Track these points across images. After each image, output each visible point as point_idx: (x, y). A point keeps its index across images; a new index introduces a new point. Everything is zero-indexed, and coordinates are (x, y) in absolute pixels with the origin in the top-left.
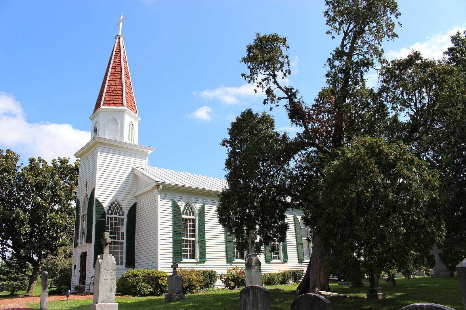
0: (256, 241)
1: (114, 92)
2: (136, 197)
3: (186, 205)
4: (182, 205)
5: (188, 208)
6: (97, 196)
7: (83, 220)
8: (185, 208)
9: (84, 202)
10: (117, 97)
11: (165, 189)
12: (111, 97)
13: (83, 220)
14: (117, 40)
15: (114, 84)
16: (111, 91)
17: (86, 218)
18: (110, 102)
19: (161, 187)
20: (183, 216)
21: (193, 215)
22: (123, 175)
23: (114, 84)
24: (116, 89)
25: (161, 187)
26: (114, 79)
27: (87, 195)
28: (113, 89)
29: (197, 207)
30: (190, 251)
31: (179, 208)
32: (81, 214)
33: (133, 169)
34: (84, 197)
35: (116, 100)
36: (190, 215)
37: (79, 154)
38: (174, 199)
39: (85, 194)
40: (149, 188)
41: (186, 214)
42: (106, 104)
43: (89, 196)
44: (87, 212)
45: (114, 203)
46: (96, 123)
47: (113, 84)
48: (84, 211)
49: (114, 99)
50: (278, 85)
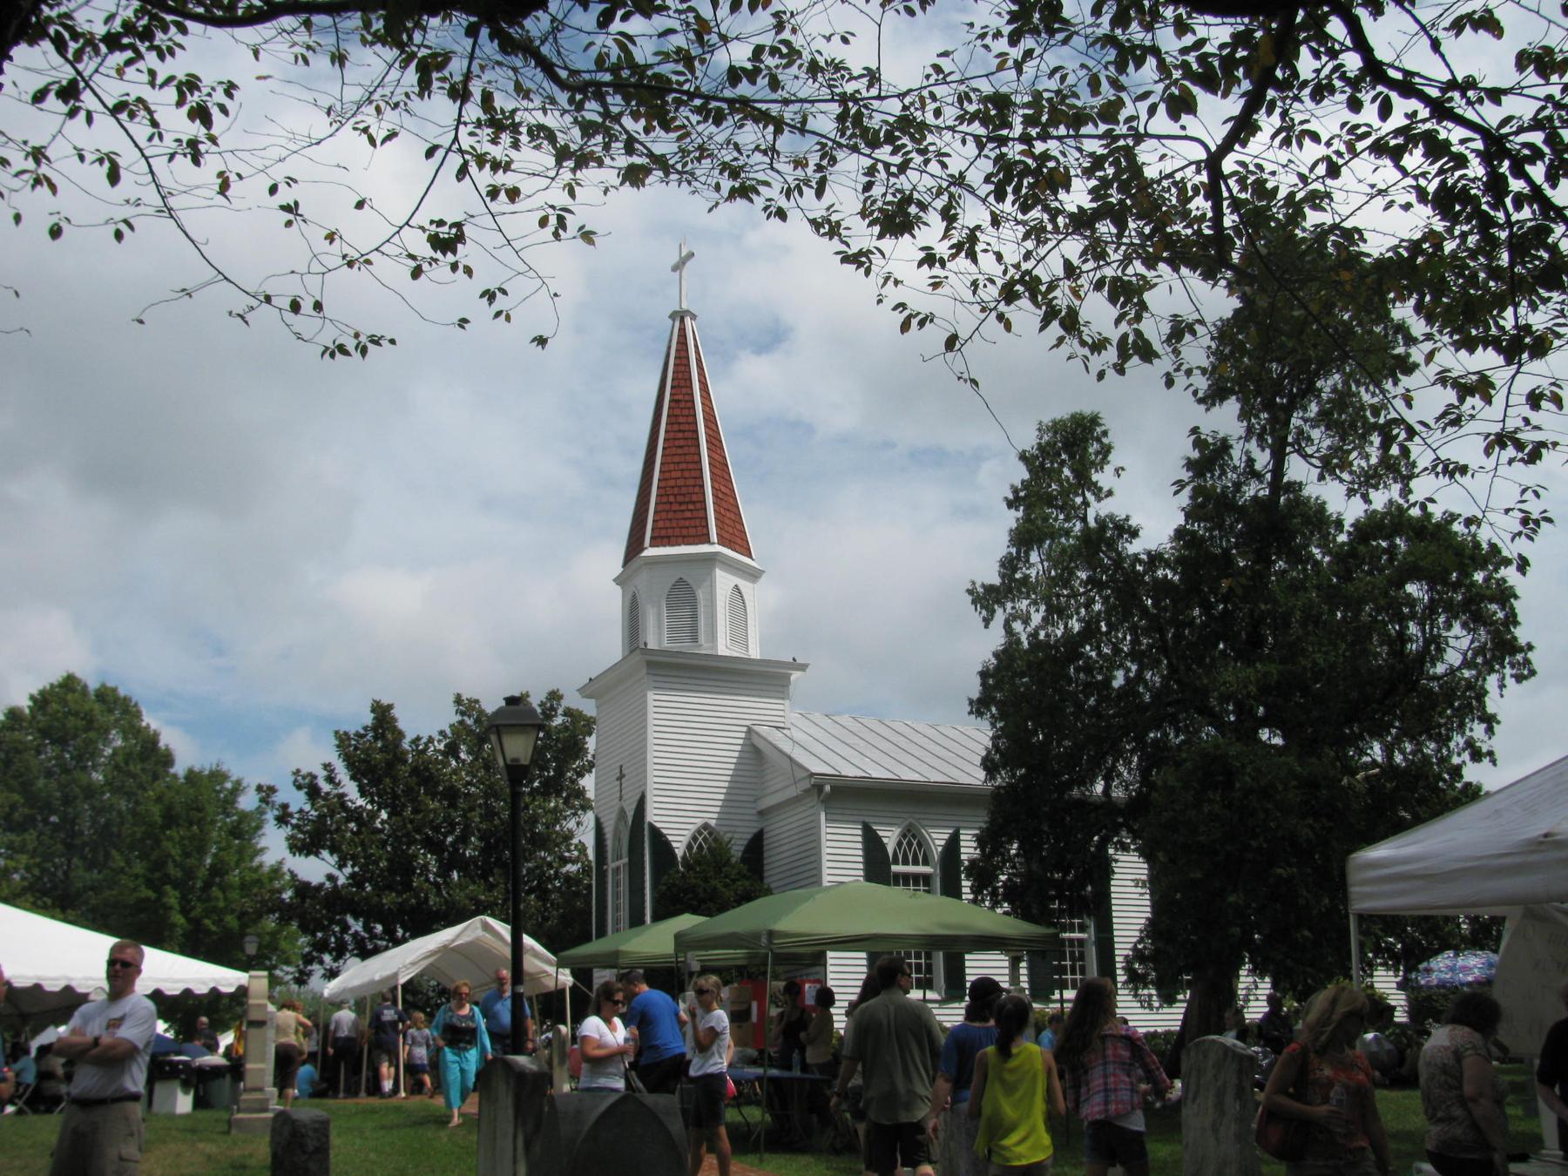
0: (1400, 1017)
1: (680, 498)
2: (761, 813)
3: (904, 836)
4: (890, 837)
5: (910, 844)
6: (653, 816)
7: (617, 884)
8: (900, 844)
9: (616, 832)
10: (688, 514)
11: (846, 796)
12: (671, 515)
13: (617, 884)
14: (677, 324)
15: (679, 474)
16: (672, 499)
17: (624, 877)
18: (670, 532)
19: (828, 788)
20: (894, 868)
21: (926, 862)
22: (724, 755)
23: (679, 474)
24: (684, 490)
25: (828, 788)
26: (676, 459)
27: (622, 812)
28: (676, 491)
29: (938, 838)
30: (918, 966)
31: (883, 847)
32: (611, 865)
33: (750, 731)
34: (614, 816)
35: (687, 523)
36: (916, 862)
37: (592, 689)
38: (867, 820)
39: (616, 809)
40: (792, 792)
41: (905, 862)
42: (657, 541)
43: (630, 814)
44: (626, 860)
45: (700, 833)
46: (634, 596)
47: (674, 475)
48: (619, 857)
49: (682, 523)
50: (1430, 37)
